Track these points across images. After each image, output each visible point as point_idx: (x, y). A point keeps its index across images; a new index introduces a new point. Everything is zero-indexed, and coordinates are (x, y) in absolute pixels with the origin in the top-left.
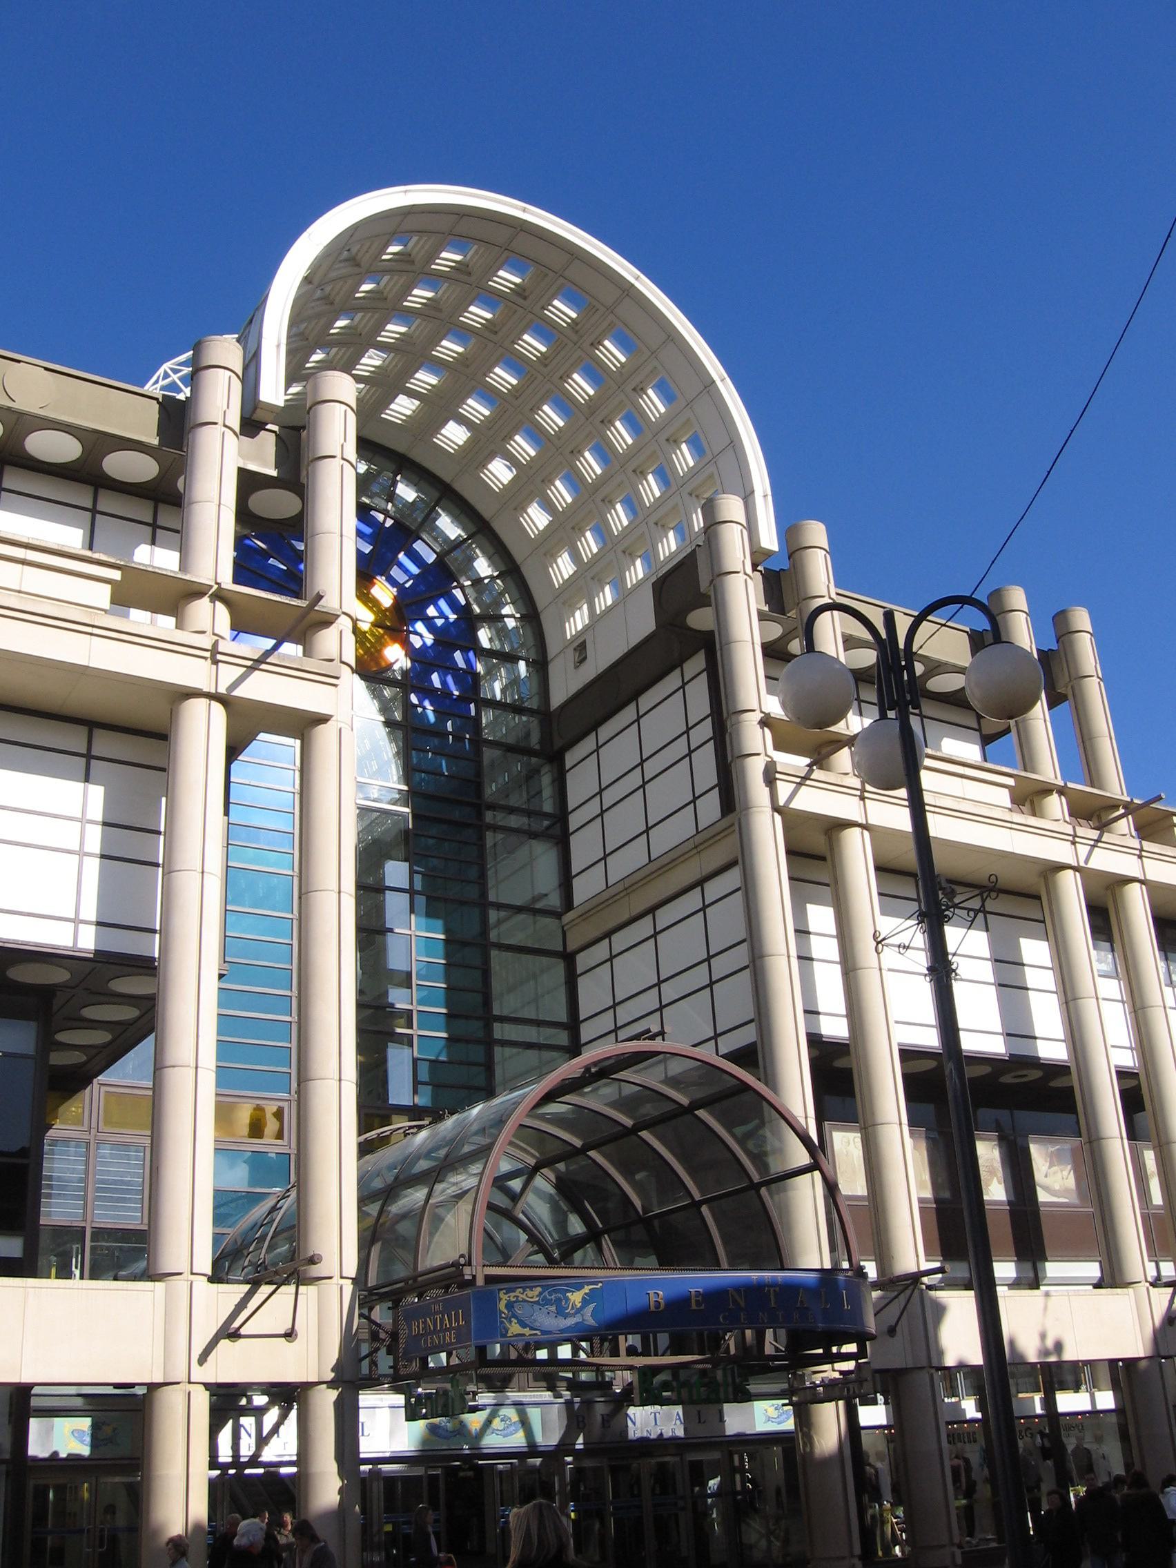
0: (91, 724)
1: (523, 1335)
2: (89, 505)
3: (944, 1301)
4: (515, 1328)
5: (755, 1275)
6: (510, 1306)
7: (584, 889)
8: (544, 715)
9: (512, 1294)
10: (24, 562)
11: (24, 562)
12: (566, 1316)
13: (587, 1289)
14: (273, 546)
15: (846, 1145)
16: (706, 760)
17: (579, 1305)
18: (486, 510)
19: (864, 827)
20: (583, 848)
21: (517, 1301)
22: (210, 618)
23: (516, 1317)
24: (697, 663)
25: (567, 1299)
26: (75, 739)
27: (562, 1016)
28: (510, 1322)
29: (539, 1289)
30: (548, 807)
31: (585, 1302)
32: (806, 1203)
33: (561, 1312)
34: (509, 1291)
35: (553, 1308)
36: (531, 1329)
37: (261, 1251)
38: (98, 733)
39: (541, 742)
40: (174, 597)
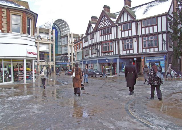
7: (62, 45)
8: (61, 36)
26: (42, 44)
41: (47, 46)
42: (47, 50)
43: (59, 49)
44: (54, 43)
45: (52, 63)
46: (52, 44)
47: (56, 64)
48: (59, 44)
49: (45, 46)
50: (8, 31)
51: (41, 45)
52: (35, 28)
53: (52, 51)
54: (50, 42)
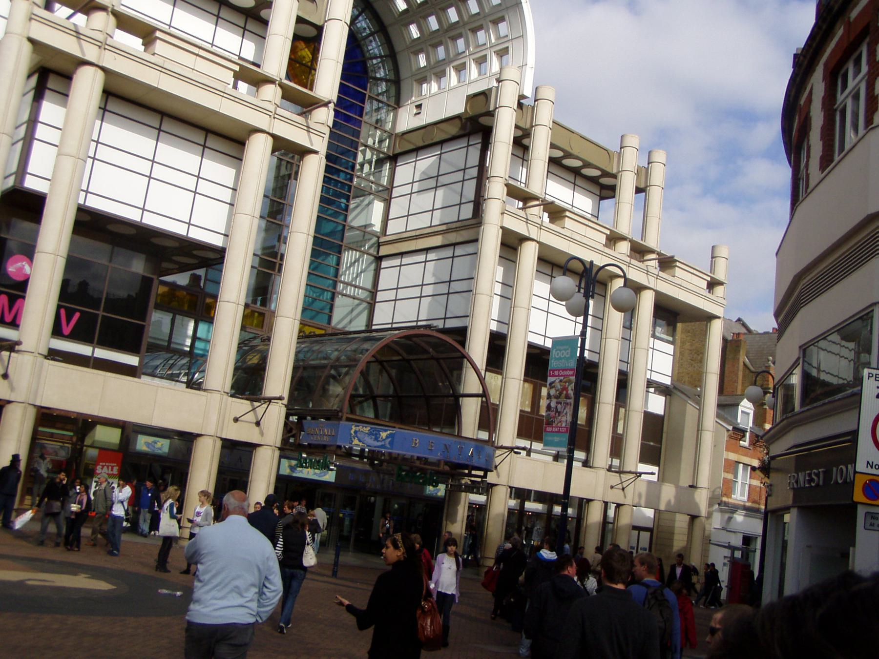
0: (208, 131)
2: (216, 13)
3: (365, 632)
4: (356, 442)
5: (99, 322)
6: (356, 432)
7: (394, 228)
10: (197, 55)
11: (197, 55)
13: (389, 432)
14: (302, 66)
15: (493, 380)
16: (470, 188)
18: (387, 20)
19: (538, 242)
20: (398, 207)
22: (271, 93)
24: (477, 140)
26: (199, 137)
27: (369, 286)
30: (385, 182)
31: (387, 437)
32: (470, 410)
33: (376, 439)
37: (248, 382)
38: (210, 136)
39: (388, 147)
40: (258, 81)
41: (218, 171)
42: (205, 224)
43: (354, 267)
44: (320, 144)
45: (242, 406)
46: (288, 154)
47: (290, 446)
48: (355, 219)
49: (179, 157)
50: (209, 341)
51: (125, 139)
52: (254, 64)
53: (269, 264)
54: (263, 112)
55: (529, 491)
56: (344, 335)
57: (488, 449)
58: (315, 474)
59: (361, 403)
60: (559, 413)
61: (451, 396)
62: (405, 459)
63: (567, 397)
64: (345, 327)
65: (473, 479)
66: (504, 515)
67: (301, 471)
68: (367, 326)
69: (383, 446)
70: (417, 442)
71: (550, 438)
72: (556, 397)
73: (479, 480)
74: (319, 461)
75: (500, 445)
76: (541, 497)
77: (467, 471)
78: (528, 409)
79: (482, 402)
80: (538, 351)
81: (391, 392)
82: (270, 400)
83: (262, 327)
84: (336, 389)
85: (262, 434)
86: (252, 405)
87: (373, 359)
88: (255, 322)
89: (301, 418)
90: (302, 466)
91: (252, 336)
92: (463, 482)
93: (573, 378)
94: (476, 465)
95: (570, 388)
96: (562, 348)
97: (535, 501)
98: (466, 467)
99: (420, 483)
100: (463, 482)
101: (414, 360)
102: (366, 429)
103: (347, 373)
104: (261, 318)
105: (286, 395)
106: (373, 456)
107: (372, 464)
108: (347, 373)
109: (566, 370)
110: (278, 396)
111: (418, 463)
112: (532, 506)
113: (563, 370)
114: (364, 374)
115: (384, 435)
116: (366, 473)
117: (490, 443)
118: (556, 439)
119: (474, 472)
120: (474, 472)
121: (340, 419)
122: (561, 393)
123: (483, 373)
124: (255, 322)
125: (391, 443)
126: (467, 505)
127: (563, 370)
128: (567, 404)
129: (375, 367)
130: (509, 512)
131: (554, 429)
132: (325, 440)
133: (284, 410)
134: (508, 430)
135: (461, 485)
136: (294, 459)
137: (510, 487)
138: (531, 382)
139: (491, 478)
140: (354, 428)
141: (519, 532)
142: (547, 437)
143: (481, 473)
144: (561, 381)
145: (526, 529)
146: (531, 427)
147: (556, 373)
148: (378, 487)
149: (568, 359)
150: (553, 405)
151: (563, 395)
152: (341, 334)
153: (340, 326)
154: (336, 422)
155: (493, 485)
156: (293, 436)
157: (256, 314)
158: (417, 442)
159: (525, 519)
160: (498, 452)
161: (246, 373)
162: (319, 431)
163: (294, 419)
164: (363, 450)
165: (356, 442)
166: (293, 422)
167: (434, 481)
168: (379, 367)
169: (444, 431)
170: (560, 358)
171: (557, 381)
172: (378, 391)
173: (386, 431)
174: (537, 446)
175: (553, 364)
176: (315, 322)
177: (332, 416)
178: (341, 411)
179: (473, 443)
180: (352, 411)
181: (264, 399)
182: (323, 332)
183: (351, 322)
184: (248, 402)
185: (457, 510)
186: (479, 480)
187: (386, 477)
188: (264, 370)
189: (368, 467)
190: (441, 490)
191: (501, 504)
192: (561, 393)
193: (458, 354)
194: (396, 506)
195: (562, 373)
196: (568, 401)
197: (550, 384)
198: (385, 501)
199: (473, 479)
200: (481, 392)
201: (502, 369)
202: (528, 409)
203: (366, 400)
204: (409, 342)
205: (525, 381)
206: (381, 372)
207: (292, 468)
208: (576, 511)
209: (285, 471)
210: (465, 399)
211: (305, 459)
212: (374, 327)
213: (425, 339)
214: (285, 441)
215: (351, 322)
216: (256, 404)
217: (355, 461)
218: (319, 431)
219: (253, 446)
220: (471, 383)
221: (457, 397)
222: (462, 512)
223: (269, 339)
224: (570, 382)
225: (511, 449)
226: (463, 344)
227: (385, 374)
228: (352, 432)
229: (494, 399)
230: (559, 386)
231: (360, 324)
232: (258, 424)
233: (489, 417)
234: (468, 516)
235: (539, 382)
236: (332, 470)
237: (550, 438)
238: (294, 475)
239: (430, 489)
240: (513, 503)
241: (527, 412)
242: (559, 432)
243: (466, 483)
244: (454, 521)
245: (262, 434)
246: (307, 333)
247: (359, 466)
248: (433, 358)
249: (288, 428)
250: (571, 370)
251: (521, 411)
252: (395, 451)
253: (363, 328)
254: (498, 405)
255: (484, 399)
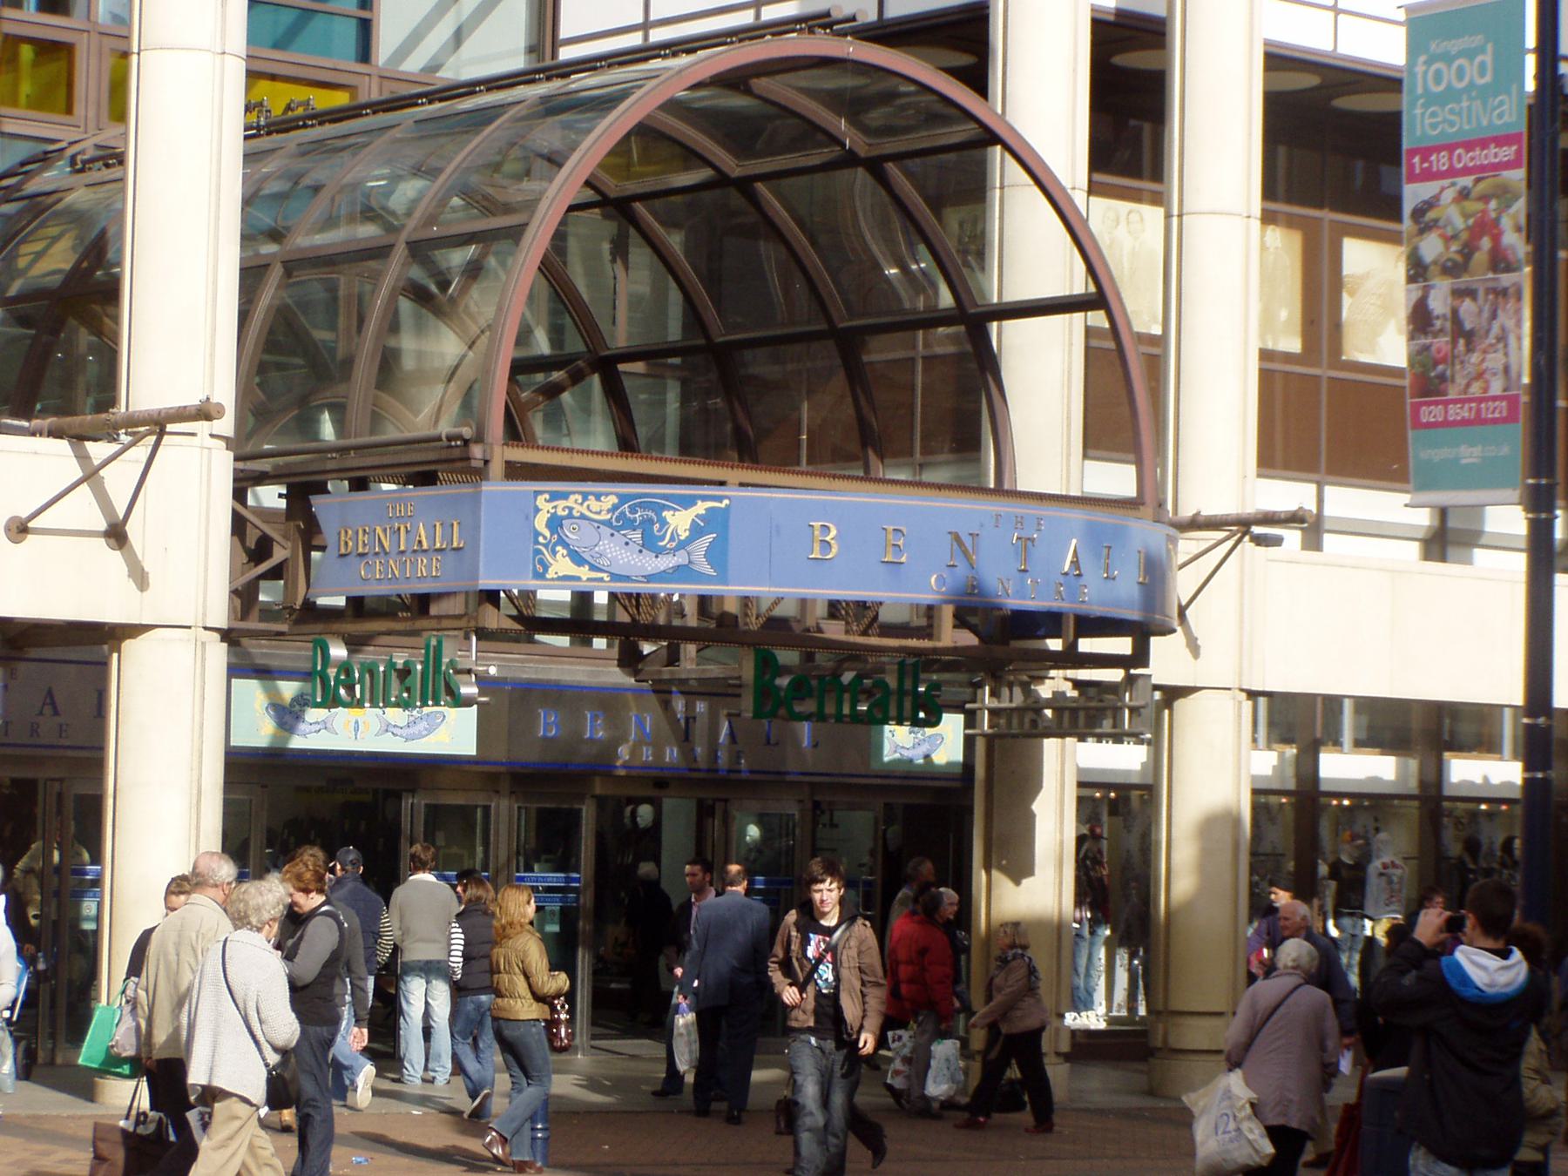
1: (578, 579)
4: (561, 565)
6: (555, 523)
9: (561, 503)
12: (659, 552)
13: (701, 508)
15: (1128, 229)
17: (684, 535)
21: (570, 516)
23: (566, 546)
25: (664, 523)
28: (554, 553)
29: (613, 500)
31: (696, 531)
32: (1041, 371)
33: (650, 544)
34: (555, 496)
35: (636, 536)
36: (593, 568)
47: (273, 621)
55: (1332, 704)
56: (443, 108)
57: (1143, 533)
58: (388, 728)
59: (552, 391)
60: (1470, 336)
61: (946, 319)
62: (778, 628)
63: (1500, 261)
64: (433, 68)
65: (1085, 674)
66: (1237, 822)
67: (325, 725)
68: (533, 49)
69: (683, 572)
70: (819, 542)
71: (1438, 454)
72: (1451, 269)
73: (1115, 675)
74: (405, 673)
75: (1186, 512)
76: (1390, 724)
77: (1055, 645)
78: (1294, 345)
79: (1089, 332)
80: (1310, 81)
81: (674, 331)
82: (159, 424)
83: (69, 110)
84: (440, 347)
85: (140, 578)
86: (83, 458)
87: (589, 195)
88: (26, 88)
89: (302, 492)
90: (332, 701)
91: (23, 150)
92: (1045, 691)
93: (1518, 176)
94: (1097, 610)
95: (1506, 222)
96: (1454, 46)
97: (1359, 744)
98: (1051, 622)
99: (856, 718)
100: (1045, 691)
101: (897, 157)
102: (602, 502)
103: (474, 271)
104: (55, 67)
105: (225, 393)
106: (632, 627)
107: (630, 659)
108: (474, 271)
109: (1484, 143)
110: (192, 400)
111: (835, 631)
112: (1349, 767)
113: (1469, 146)
114: (552, 269)
115: (680, 521)
116: (606, 701)
117: (1148, 510)
118: (1470, 454)
119: (1086, 645)
120: (1086, 645)
121: (481, 473)
122: (1468, 251)
123: (1080, 198)
124: (26, 88)
125: (717, 555)
126: (1071, 794)
127: (1469, 146)
128: (1502, 293)
129: (597, 229)
130: (1257, 809)
131: (1456, 413)
132: (423, 575)
133: (223, 465)
134: (1215, 442)
135: (1036, 706)
136: (288, 675)
137: (1252, 695)
138: (1291, 223)
139: (1167, 661)
140: (545, 507)
141: (1305, 888)
142: (1422, 450)
143: (1122, 645)
144: (1464, 195)
145: (1336, 869)
146: (1324, 420)
147: (1441, 161)
148: (671, 754)
149: (1485, 93)
150: (1439, 303)
151: (1481, 257)
152: (433, 96)
153: (413, 64)
154: (466, 490)
155: (1173, 694)
156: (276, 573)
157: (26, 52)
158: (819, 542)
159: (1325, 829)
160: (1188, 545)
161: (23, 321)
162: (383, 540)
163: (271, 497)
164: (583, 599)
165: (561, 565)
166: (266, 514)
167: (921, 702)
168: (610, 228)
169: (929, 476)
170: (1450, 95)
171: (1449, 195)
172: (620, 337)
173: (687, 502)
174: (1346, 501)
175: (1420, 125)
176: (298, 57)
177: (429, 467)
178: (479, 438)
179: (1077, 515)
180: (515, 432)
181: (132, 422)
182: (340, 99)
183: (458, 38)
184: (63, 445)
185: (1030, 818)
186: (1115, 675)
187: (701, 707)
188: (110, 293)
189: (615, 676)
190: (946, 743)
191: (1215, 772)
192: (1468, 251)
193: (960, 133)
194: (753, 832)
195: (1465, 159)
196: (1506, 279)
197: (1418, 213)
198: (704, 811)
199: (1085, 674)
200: (1077, 283)
201: (1157, 171)
202: (1294, 345)
203: (577, 378)
204: (737, 101)
205: (1268, 218)
206: (620, 250)
207: (288, 716)
208: (734, 836)
209: (257, 731)
210: (1010, 325)
211: (346, 668)
212: (566, 54)
213: (804, 79)
214: (244, 597)
215: (458, 38)
216: (98, 450)
217: (556, 654)
218: (383, 540)
219: (92, 644)
220: (1028, 250)
221: (976, 321)
222: (1054, 823)
223: (114, 158)
224: (1504, 195)
225: (1246, 527)
226: (978, 79)
227: (640, 254)
228: (540, 522)
229: (1143, 314)
230: (1455, 217)
231: (500, 46)
232: (116, 534)
233: (1126, 397)
234: (1080, 840)
235: (1327, 215)
236: (467, 702)
237: (1438, 454)
238: (297, 743)
239: (899, 742)
240: (1266, 763)
241: (1288, 357)
242: (1479, 421)
243: (1059, 696)
244: (1020, 869)
245: (140, 578)
246: (277, 111)
247: (576, 673)
248: (850, 160)
249: (250, 540)
250: (1501, 141)
251: (1266, 355)
252: (730, 591)
253: (518, 63)
254: (1161, 341)
255: (1098, 319)
